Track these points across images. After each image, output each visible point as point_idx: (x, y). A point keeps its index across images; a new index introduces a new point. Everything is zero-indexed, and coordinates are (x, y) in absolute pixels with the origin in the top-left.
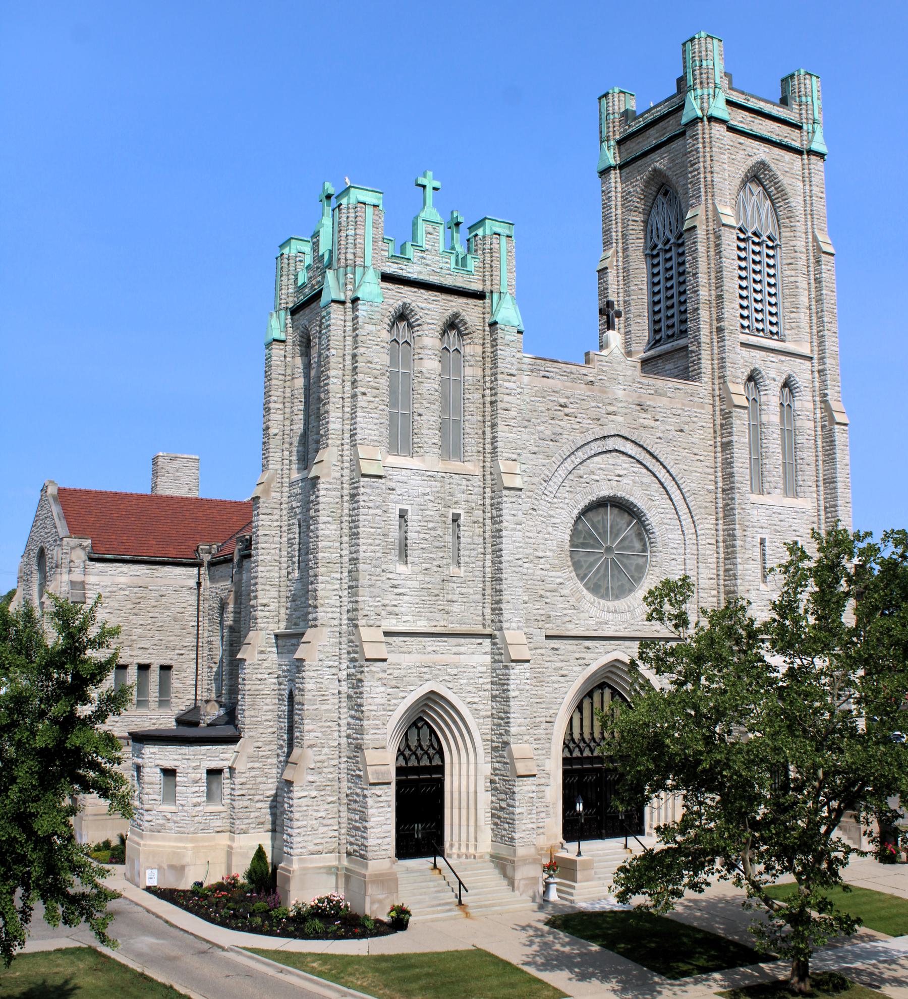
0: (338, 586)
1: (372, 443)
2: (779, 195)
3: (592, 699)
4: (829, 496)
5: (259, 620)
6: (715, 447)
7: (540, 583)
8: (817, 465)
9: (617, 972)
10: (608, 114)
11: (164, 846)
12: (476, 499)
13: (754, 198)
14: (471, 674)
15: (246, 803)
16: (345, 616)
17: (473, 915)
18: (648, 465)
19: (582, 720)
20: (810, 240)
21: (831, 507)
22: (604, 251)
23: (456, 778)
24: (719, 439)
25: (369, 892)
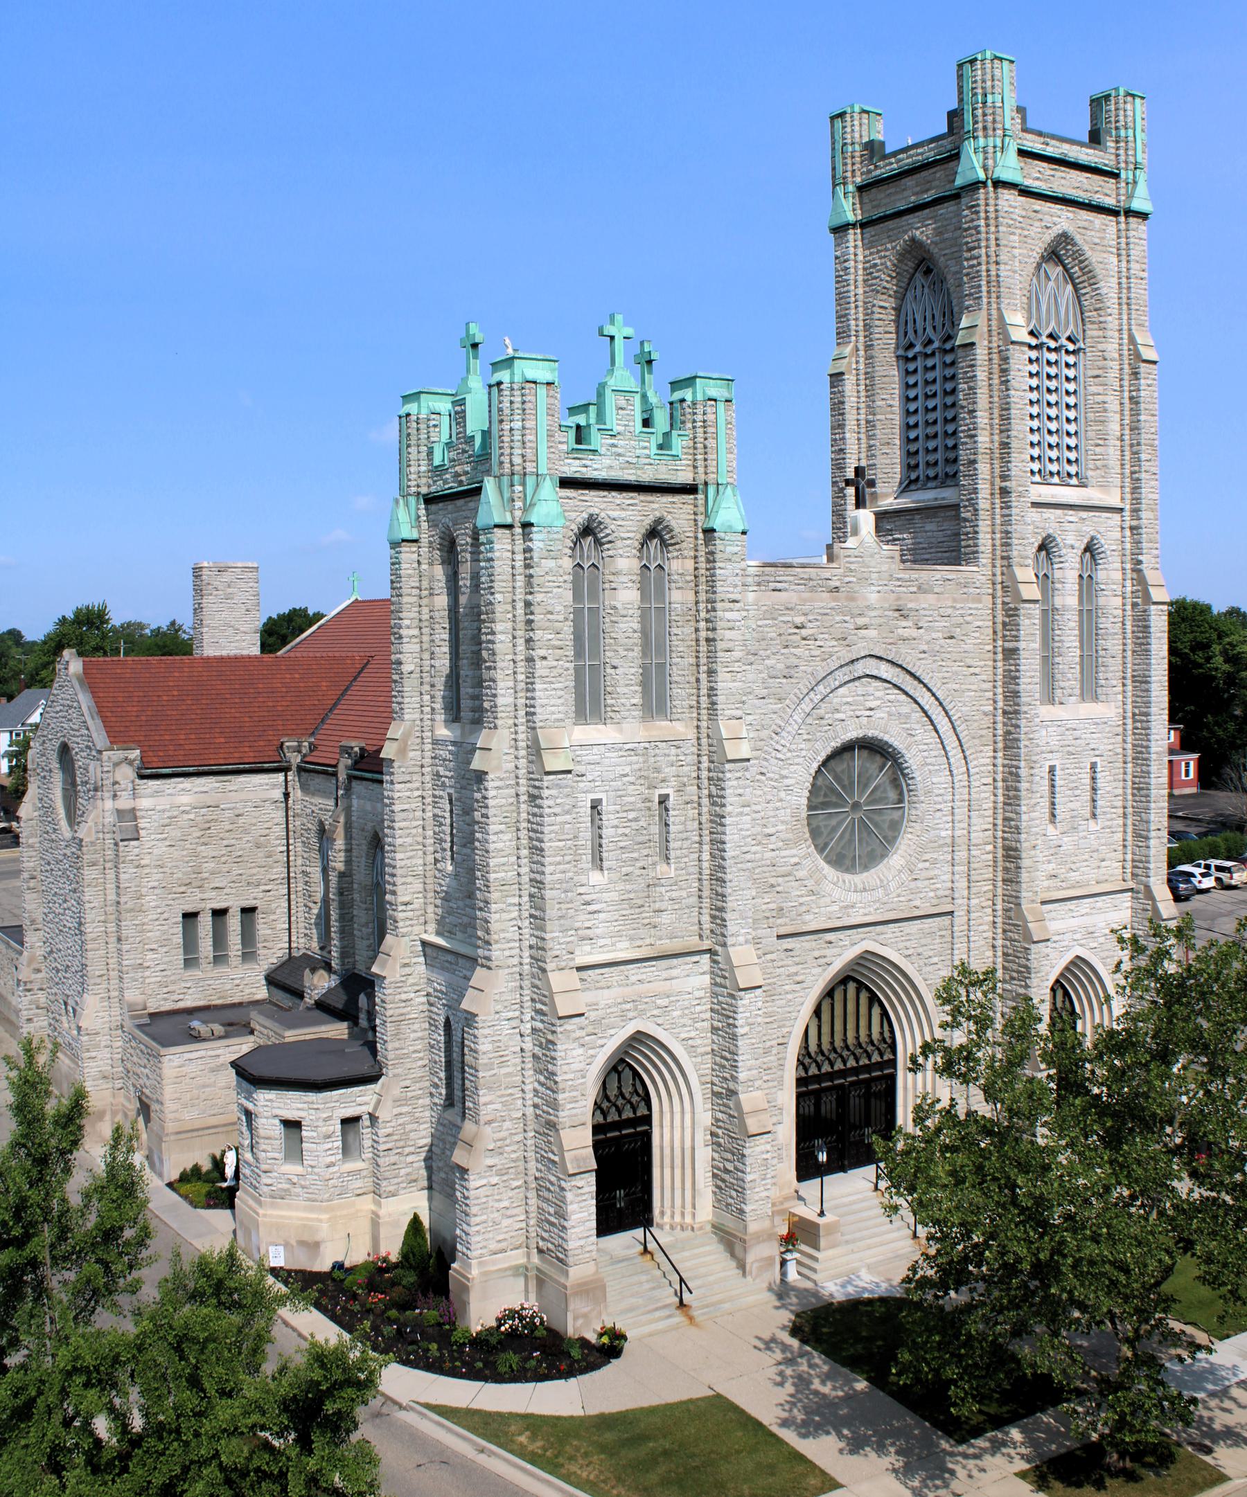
0: (516, 914)
1: (557, 724)
2: (1085, 278)
3: (833, 999)
4: (1138, 699)
5: (400, 924)
6: (995, 653)
7: (771, 868)
8: (1124, 657)
9: (896, 1434)
10: (845, 144)
11: (290, 1218)
12: (690, 771)
13: (1051, 284)
14: (686, 1003)
15: (393, 1159)
16: (526, 953)
17: (698, 1319)
18: (907, 689)
19: (819, 1027)
20: (1126, 341)
21: (1141, 714)
22: (838, 344)
23: (667, 1130)
24: (1000, 643)
25: (571, 1307)
